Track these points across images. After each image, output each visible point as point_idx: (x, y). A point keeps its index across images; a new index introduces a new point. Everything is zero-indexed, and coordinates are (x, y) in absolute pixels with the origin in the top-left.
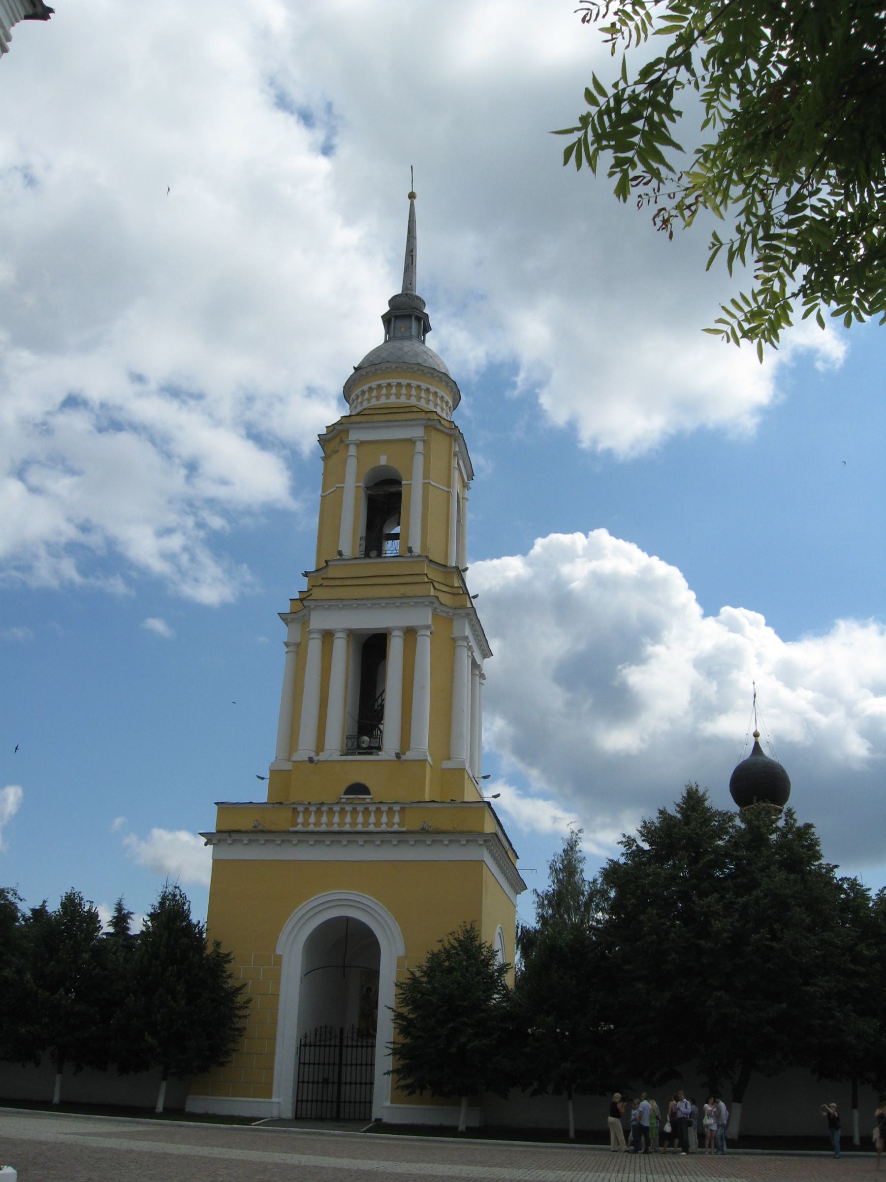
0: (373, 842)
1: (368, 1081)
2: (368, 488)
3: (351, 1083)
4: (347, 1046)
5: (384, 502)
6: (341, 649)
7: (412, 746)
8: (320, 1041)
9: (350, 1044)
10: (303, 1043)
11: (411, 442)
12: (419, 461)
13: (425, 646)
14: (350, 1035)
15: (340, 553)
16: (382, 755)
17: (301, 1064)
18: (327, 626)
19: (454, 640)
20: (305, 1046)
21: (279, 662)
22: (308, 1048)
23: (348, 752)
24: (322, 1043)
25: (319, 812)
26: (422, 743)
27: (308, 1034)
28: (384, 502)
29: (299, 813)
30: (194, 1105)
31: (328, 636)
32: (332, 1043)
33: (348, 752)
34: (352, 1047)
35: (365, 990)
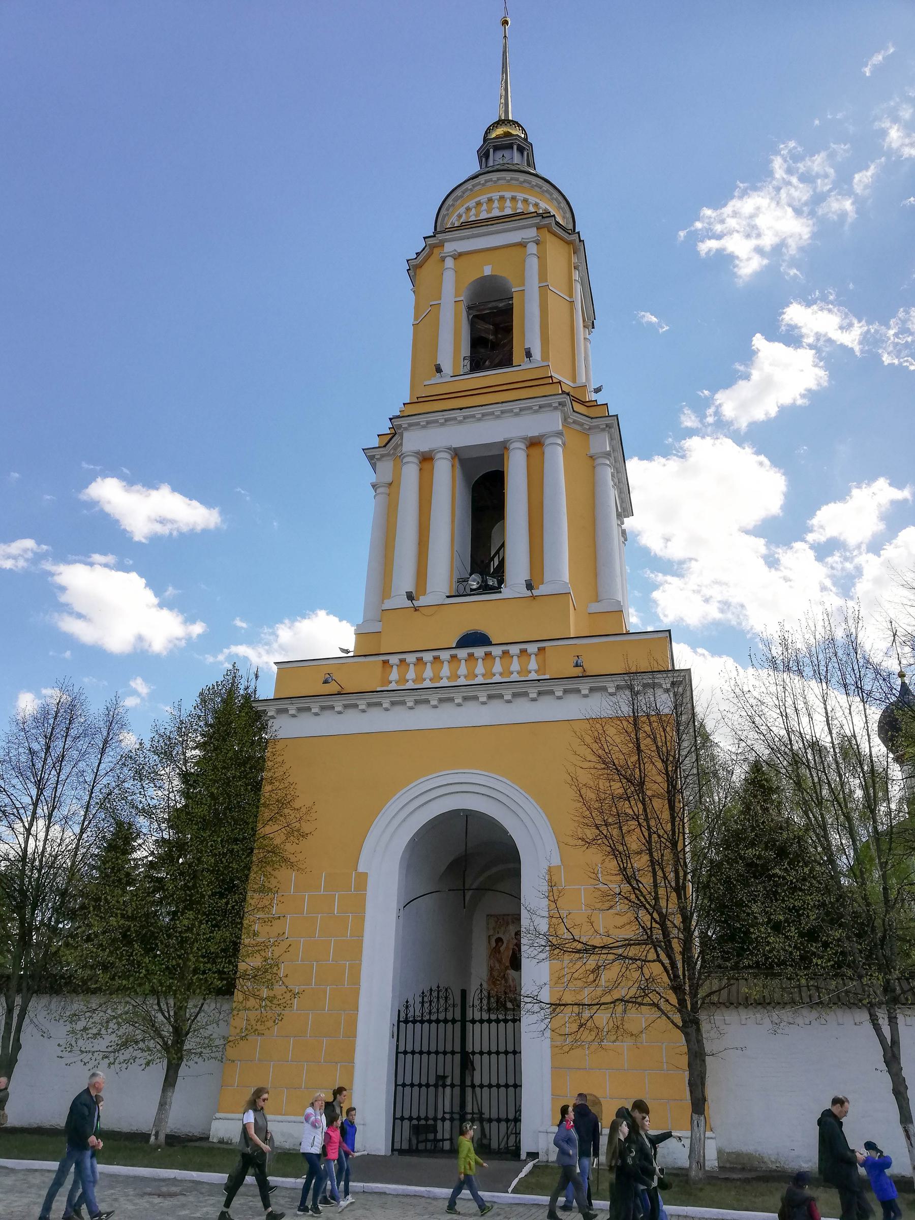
1: (510, 1049)
2: (469, 308)
4: (473, 1022)
5: (491, 332)
6: (444, 473)
7: (546, 579)
8: (430, 1013)
9: (477, 1017)
10: (403, 1015)
11: (522, 245)
12: (533, 264)
13: (557, 458)
14: (477, 1002)
15: (439, 370)
16: (507, 592)
17: (399, 1086)
18: (424, 448)
20: (406, 1022)
21: (365, 507)
22: (410, 1025)
23: (460, 590)
24: (434, 1017)
26: (561, 569)
27: (411, 1002)
28: (491, 332)
31: (426, 459)
32: (450, 1017)
33: (477, 364)
34: (481, 1021)
35: (493, 944)
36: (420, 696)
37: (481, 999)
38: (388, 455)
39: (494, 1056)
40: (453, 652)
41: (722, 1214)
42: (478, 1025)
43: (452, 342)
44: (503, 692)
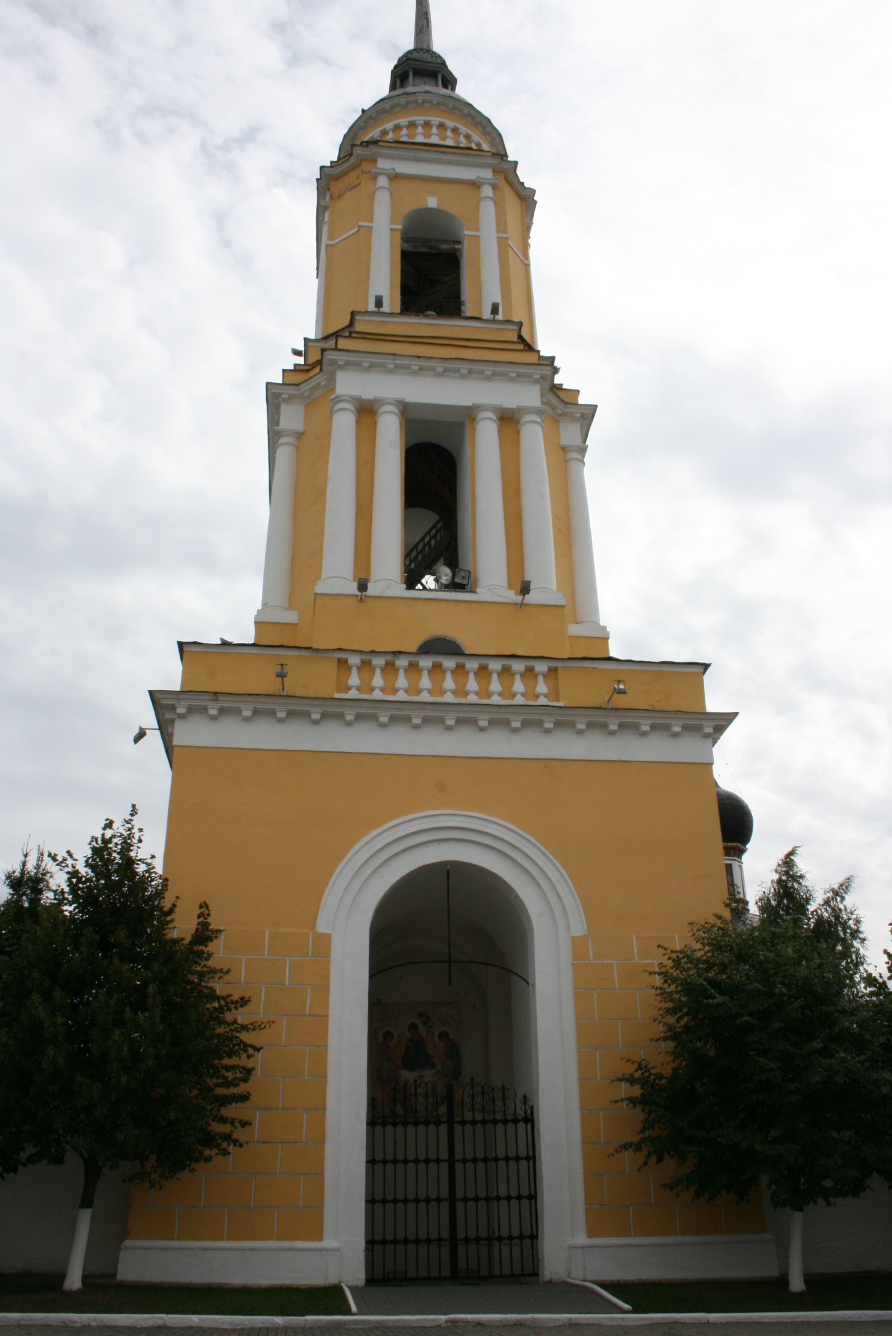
0: (273, 713)
3: (477, 1199)
8: (473, 1109)
11: (475, 185)
13: (534, 438)
14: (467, 1100)
19: (564, 449)
25: (390, 668)
28: (432, 274)
29: (349, 668)
30: (144, 1260)
31: (366, 411)
34: (474, 1123)
35: (381, 1038)
36: (367, 713)
37: (473, 1096)
38: (301, 396)
39: (400, 1166)
40: (413, 659)
41: (882, 1315)
42: (469, 1128)
43: (383, 278)
44: (312, 710)
